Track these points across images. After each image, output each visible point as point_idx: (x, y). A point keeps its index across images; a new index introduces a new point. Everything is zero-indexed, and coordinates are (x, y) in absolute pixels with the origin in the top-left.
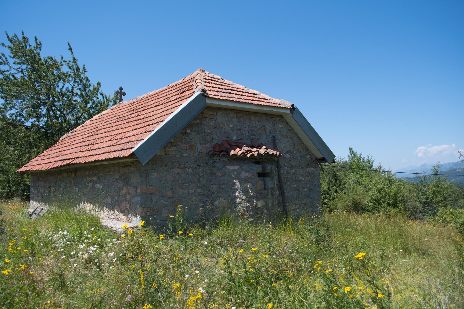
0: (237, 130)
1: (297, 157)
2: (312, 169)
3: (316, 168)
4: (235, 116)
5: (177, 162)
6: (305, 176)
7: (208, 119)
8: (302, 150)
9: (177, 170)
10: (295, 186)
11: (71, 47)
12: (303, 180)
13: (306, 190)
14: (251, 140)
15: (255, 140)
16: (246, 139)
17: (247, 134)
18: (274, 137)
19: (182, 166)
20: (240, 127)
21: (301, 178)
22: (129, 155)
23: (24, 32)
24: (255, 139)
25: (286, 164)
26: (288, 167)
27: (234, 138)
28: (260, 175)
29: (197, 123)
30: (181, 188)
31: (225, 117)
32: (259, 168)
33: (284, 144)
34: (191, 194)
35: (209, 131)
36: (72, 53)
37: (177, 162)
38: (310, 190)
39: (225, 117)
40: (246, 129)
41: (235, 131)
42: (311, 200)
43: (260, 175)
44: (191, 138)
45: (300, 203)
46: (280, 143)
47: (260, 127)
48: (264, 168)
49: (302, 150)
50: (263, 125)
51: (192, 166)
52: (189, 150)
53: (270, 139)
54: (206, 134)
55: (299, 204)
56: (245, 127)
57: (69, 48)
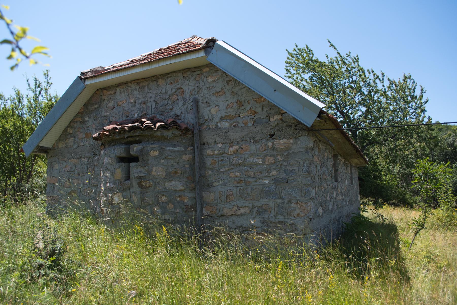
0: (141, 104)
1: (246, 124)
2: (283, 141)
3: (296, 138)
4: (138, 87)
5: (74, 152)
6: (265, 156)
7: (106, 101)
8: (259, 110)
9: (74, 161)
10: (238, 174)
11: (332, 43)
12: (257, 164)
13: (267, 182)
14: (161, 113)
15: (167, 111)
16: (153, 112)
17: (154, 106)
18: (196, 102)
19: (77, 156)
20: (143, 100)
21: (251, 160)
22: (130, 150)
23: (297, 45)
24: (166, 109)
25: (218, 139)
26: (222, 144)
27: (136, 115)
28: (121, 160)
29: (96, 108)
30: (77, 179)
31: (124, 93)
32: (120, 151)
33: (217, 107)
34: (85, 185)
35: (106, 114)
36: (335, 48)
37: (74, 152)
38: (276, 181)
39: (124, 93)
40: (153, 99)
41: (137, 106)
42: (279, 201)
43: (121, 160)
44: (88, 125)
45: (251, 205)
46: (210, 106)
47: (174, 90)
48: (128, 151)
49: (259, 110)
50: (178, 86)
51: (86, 155)
52: (86, 139)
53: (190, 105)
54: (103, 118)
55: (249, 207)
56: (151, 98)
57: (329, 44)
